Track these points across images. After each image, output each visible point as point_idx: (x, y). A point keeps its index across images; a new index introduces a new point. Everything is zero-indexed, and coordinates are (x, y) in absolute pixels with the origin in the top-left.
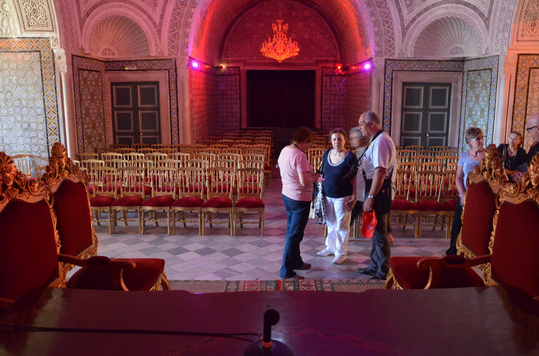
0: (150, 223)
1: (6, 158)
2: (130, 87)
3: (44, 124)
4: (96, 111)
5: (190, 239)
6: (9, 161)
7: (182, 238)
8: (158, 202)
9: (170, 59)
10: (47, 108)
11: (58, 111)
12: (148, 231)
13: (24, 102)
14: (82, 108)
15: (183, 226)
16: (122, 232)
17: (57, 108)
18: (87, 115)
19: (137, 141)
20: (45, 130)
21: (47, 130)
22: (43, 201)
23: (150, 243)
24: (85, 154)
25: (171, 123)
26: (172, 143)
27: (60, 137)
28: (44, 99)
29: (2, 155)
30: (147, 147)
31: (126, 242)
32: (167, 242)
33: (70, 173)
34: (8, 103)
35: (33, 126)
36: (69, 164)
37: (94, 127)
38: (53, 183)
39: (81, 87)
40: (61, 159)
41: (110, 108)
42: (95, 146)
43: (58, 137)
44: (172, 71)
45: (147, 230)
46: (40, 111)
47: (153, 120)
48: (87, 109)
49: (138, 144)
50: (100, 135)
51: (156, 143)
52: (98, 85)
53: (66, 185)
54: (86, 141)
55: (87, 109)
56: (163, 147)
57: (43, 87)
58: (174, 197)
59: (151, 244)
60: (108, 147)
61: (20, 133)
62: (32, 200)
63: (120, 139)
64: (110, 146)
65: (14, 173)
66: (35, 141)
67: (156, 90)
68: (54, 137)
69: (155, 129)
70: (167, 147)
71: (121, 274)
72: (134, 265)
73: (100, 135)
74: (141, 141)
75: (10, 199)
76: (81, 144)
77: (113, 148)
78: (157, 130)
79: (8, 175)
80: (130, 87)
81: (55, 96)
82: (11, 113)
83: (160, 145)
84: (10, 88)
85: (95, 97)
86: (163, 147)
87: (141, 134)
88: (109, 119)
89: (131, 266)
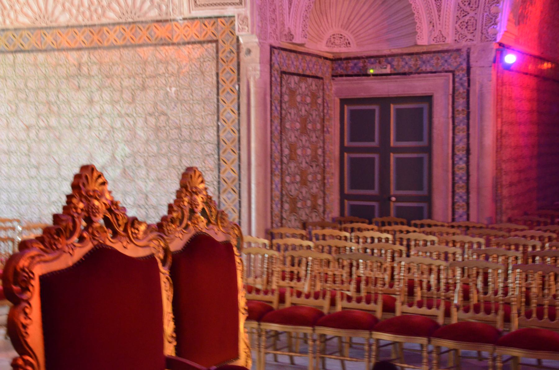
3: (216, 173)
4: (309, 152)
6: (100, 180)
10: (222, 143)
11: (239, 149)
13: (186, 133)
14: (285, 144)
18: (291, 158)
19: (385, 212)
20: (216, 183)
21: (219, 183)
24: (283, 230)
25: (453, 179)
26: (453, 220)
27: (240, 197)
28: (218, 127)
29: (90, 169)
33: (209, 222)
34: (160, 134)
36: (210, 207)
37: (304, 182)
39: (283, 105)
42: (304, 218)
46: (210, 148)
47: (417, 172)
48: (292, 148)
49: (385, 219)
50: (314, 197)
51: (421, 219)
52: (316, 103)
53: (199, 242)
54: (286, 206)
55: (292, 148)
56: (436, 225)
57: (218, 106)
60: (329, 220)
62: (132, 251)
63: (352, 207)
70: (442, 226)
74: (392, 212)
76: (277, 211)
77: (339, 223)
79: (96, 203)
81: (237, 121)
84: (164, 108)
85: (310, 126)
86: (436, 225)
87: (393, 199)
88: (333, 168)
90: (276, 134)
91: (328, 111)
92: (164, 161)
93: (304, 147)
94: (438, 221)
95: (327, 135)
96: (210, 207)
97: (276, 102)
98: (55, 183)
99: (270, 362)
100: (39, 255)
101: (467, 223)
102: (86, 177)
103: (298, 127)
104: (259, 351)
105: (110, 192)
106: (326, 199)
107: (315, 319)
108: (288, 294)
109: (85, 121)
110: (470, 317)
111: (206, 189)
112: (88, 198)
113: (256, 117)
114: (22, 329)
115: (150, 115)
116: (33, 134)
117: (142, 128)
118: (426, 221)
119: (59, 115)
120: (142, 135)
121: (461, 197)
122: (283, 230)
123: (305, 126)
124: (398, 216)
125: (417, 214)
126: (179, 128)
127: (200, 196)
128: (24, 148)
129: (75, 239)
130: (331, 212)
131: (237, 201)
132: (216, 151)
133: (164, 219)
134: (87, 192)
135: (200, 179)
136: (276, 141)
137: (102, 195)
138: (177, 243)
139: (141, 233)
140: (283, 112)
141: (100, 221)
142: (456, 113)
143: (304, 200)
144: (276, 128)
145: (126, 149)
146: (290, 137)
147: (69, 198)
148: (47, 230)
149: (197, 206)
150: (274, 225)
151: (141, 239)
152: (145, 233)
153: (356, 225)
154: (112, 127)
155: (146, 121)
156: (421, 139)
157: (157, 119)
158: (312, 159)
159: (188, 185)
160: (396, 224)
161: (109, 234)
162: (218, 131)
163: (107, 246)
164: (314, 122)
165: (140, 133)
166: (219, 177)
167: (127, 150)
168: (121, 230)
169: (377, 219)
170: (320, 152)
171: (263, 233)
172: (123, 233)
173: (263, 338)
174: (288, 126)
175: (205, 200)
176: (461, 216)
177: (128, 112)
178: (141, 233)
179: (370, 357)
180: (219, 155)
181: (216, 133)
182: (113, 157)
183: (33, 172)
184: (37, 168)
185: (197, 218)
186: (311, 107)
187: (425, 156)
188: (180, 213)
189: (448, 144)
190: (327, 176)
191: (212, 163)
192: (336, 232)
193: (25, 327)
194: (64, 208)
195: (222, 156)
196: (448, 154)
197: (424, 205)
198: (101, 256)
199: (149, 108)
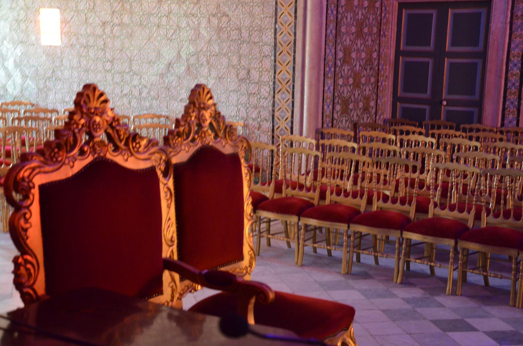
0: (417, 265)
1: (97, 94)
2: (434, 12)
3: (272, 73)
4: (363, 55)
5: (488, 309)
6: (102, 99)
7: (471, 304)
8: (436, 228)
10: (278, 45)
11: (295, 52)
12: (411, 280)
13: (245, 34)
14: (339, 47)
15: (482, 283)
16: (365, 276)
17: (295, 47)
18: (346, 60)
19: (435, 115)
20: (271, 83)
21: (274, 83)
22: (151, 172)
23: (407, 301)
24: (332, 131)
25: (506, 85)
26: (502, 125)
27: (293, 97)
28: (276, 29)
29: (92, 88)
30: (451, 128)
31: (364, 293)
32: (441, 306)
33: (216, 136)
34: (221, 34)
35: (255, 75)
36: (218, 122)
37: (357, 85)
38: (183, 147)
39: (340, 9)
40: (204, 112)
41: (393, 51)
42: (355, 118)
43: (291, 97)
45: (409, 278)
46: (268, 50)
47: (470, 78)
48: (347, 51)
49: (436, 122)
50: (367, 99)
51: (471, 123)
52: (374, 7)
53: (206, 156)
54: (338, 107)
55: (347, 51)
56: (484, 130)
57: (276, 9)
58: (470, 224)
59: (408, 302)
60: (380, 122)
61: (233, 86)
62: (133, 163)
63: (404, 110)
64: (385, 121)
65: (108, 119)
66: (254, 100)
68: (284, 96)
69: (474, 94)
70: (491, 131)
71: (251, 307)
72: (272, 296)
73: (367, 99)
74: (443, 116)
75: (96, 156)
76: (328, 112)
77: (390, 125)
78: (477, 97)
79: (98, 119)
80: (434, 12)
81: (293, 24)
82: (224, 51)
83: (478, 126)
84: (226, 9)
85: (366, 30)
86: (484, 130)
87: (445, 103)
88: (388, 71)
89: (266, 296)
90: (331, 37)
91: (385, 15)
92: (225, 61)
93: (358, 51)
94: (487, 126)
95: (383, 39)
96: (218, 122)
97: (333, 6)
98: (127, 77)
99: (310, 253)
100: (39, 167)
101: (516, 129)
102: (88, 96)
103: (353, 31)
104: (299, 244)
105: (112, 109)
106: (379, 101)
107: (351, 216)
108: (328, 193)
109: (154, 20)
110: (500, 222)
111: (215, 105)
112: (90, 115)
113: (312, 21)
114: (23, 233)
115: (214, 16)
116: (108, 30)
117: (206, 28)
118: (475, 126)
119: (132, 13)
120: (205, 34)
121: (512, 103)
122: (332, 131)
123: (361, 30)
124: (448, 119)
125: (467, 119)
126: (239, 29)
127: (209, 111)
128: (100, 43)
129: (76, 151)
130: (382, 113)
131: (291, 100)
132: (273, 53)
133: (171, 132)
134: (89, 109)
135: (209, 96)
136: (331, 44)
137: (103, 113)
138: (182, 155)
139: (142, 147)
140: (339, 16)
141: (101, 136)
142: (514, 18)
143: (356, 102)
144: (331, 32)
145: (191, 47)
146: (346, 40)
147: (72, 114)
148: (48, 144)
149: (205, 120)
150: (325, 125)
151: (142, 152)
152: (146, 146)
153: (405, 128)
154: (178, 26)
155: (209, 21)
156: (476, 44)
157: (220, 20)
158: (366, 62)
159: (196, 101)
160: (446, 127)
161: (111, 147)
162: (275, 34)
163: (109, 160)
164: (370, 27)
165: (204, 32)
166: (274, 77)
167: (192, 49)
168: (122, 145)
169: (427, 121)
170: (375, 55)
171: (313, 133)
172: (123, 147)
173: (302, 231)
174: (343, 29)
175: (213, 115)
176: (510, 122)
177: (193, 12)
178: (142, 147)
179: (399, 253)
180: (275, 56)
181: (273, 36)
182: (179, 56)
183: (108, 66)
184: (112, 62)
185: (205, 133)
186: (368, 11)
187: (479, 61)
188: (187, 127)
189: (504, 50)
190: (381, 79)
191: (268, 63)
192: (382, 135)
193: (26, 230)
194: (66, 123)
195: (278, 58)
196: (503, 60)
197: (475, 110)
198: (101, 168)
199: (212, 8)
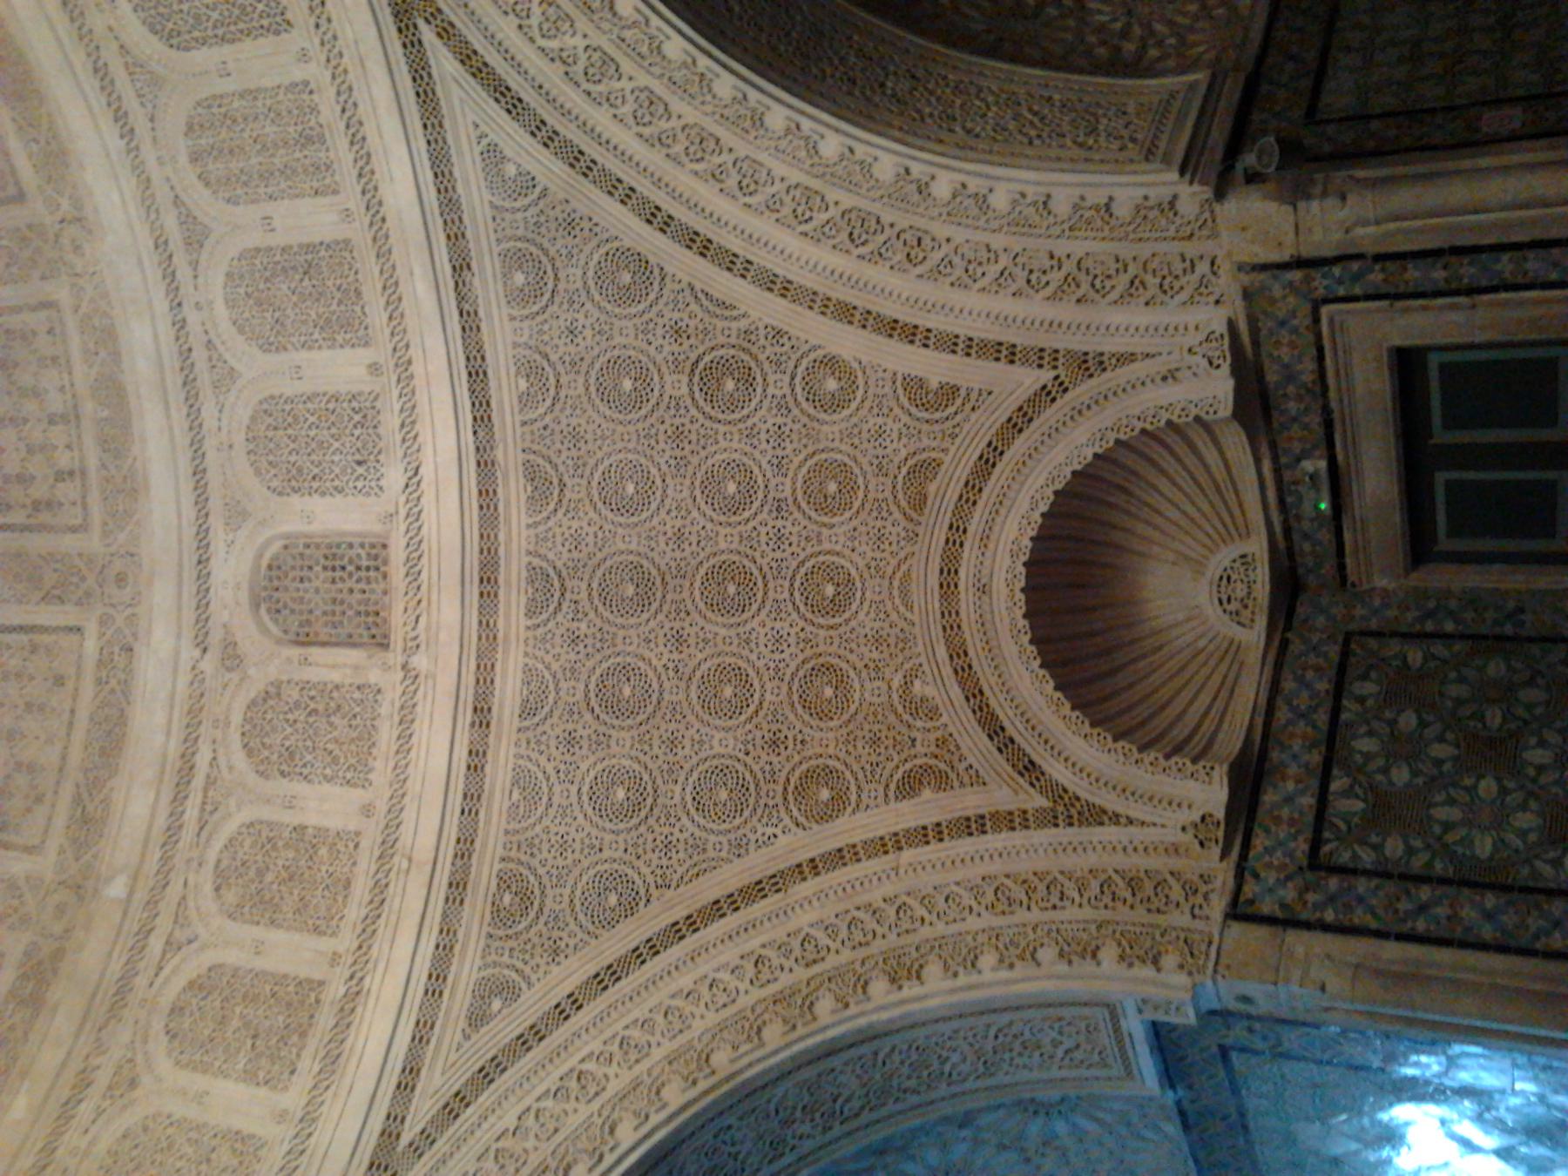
9: (1247, 295)
44: (1320, 283)
67: (1540, 545)
